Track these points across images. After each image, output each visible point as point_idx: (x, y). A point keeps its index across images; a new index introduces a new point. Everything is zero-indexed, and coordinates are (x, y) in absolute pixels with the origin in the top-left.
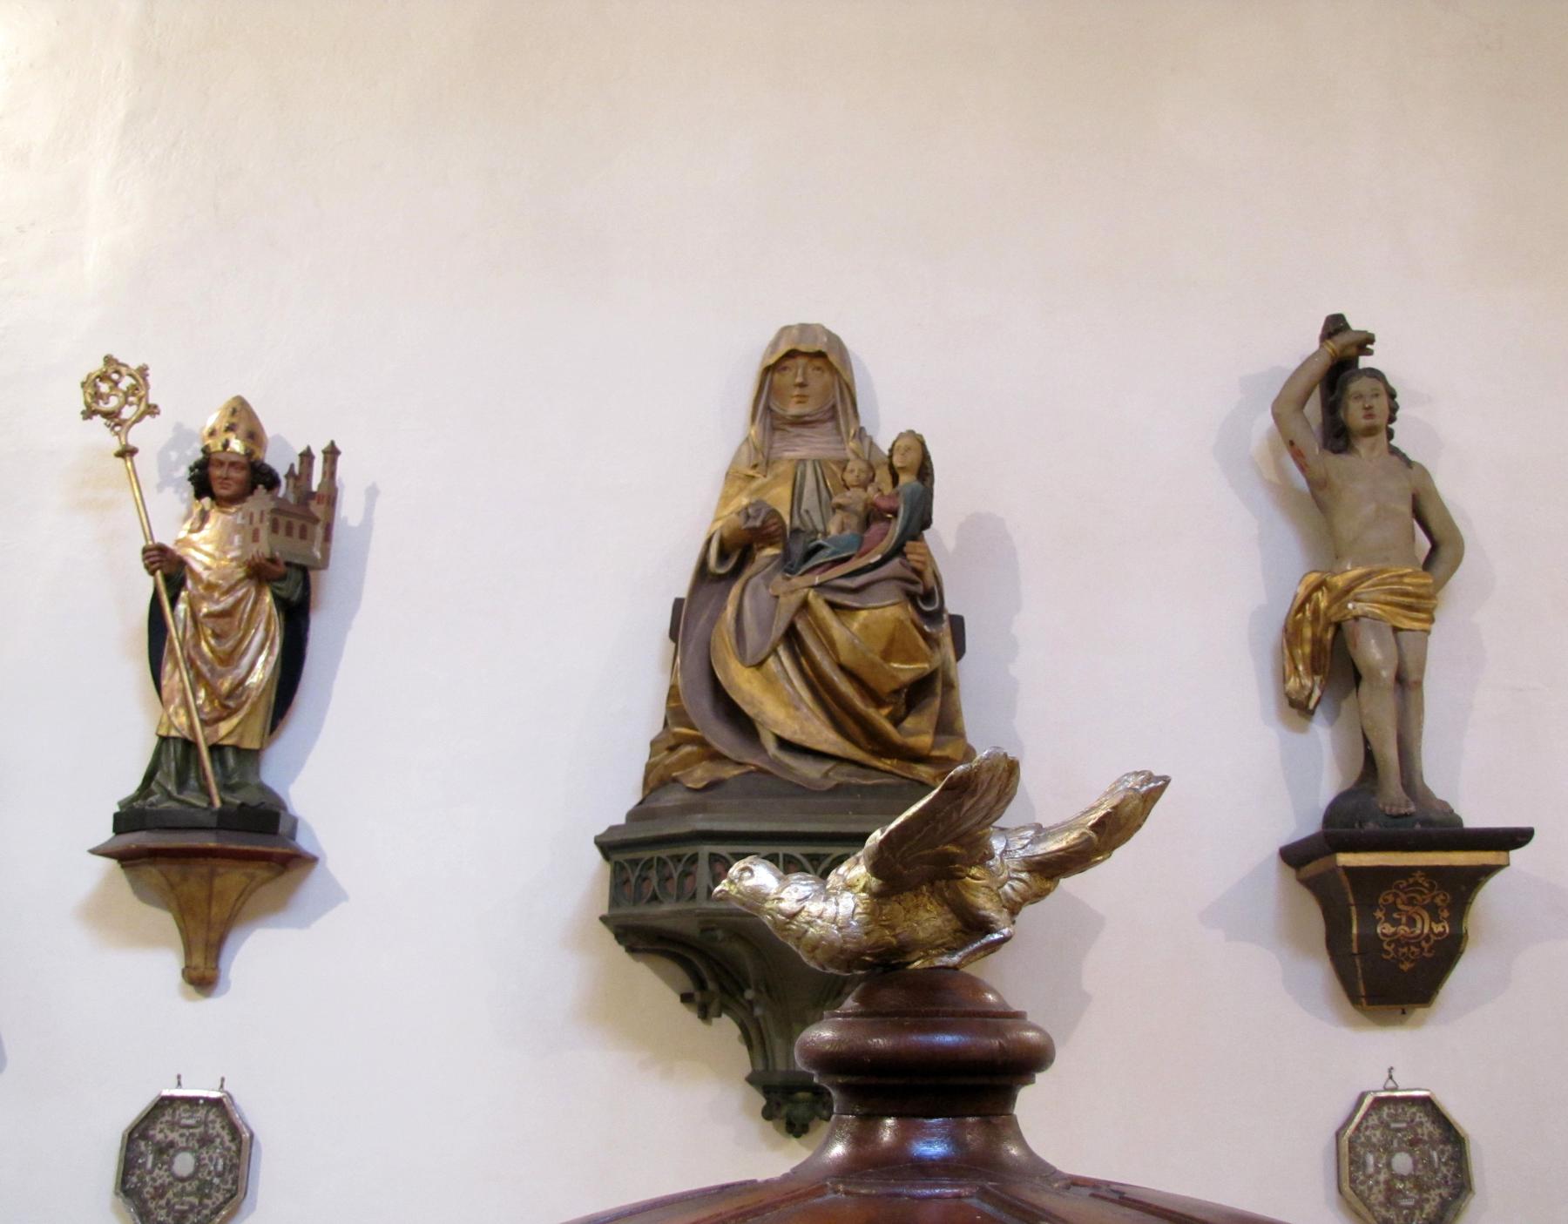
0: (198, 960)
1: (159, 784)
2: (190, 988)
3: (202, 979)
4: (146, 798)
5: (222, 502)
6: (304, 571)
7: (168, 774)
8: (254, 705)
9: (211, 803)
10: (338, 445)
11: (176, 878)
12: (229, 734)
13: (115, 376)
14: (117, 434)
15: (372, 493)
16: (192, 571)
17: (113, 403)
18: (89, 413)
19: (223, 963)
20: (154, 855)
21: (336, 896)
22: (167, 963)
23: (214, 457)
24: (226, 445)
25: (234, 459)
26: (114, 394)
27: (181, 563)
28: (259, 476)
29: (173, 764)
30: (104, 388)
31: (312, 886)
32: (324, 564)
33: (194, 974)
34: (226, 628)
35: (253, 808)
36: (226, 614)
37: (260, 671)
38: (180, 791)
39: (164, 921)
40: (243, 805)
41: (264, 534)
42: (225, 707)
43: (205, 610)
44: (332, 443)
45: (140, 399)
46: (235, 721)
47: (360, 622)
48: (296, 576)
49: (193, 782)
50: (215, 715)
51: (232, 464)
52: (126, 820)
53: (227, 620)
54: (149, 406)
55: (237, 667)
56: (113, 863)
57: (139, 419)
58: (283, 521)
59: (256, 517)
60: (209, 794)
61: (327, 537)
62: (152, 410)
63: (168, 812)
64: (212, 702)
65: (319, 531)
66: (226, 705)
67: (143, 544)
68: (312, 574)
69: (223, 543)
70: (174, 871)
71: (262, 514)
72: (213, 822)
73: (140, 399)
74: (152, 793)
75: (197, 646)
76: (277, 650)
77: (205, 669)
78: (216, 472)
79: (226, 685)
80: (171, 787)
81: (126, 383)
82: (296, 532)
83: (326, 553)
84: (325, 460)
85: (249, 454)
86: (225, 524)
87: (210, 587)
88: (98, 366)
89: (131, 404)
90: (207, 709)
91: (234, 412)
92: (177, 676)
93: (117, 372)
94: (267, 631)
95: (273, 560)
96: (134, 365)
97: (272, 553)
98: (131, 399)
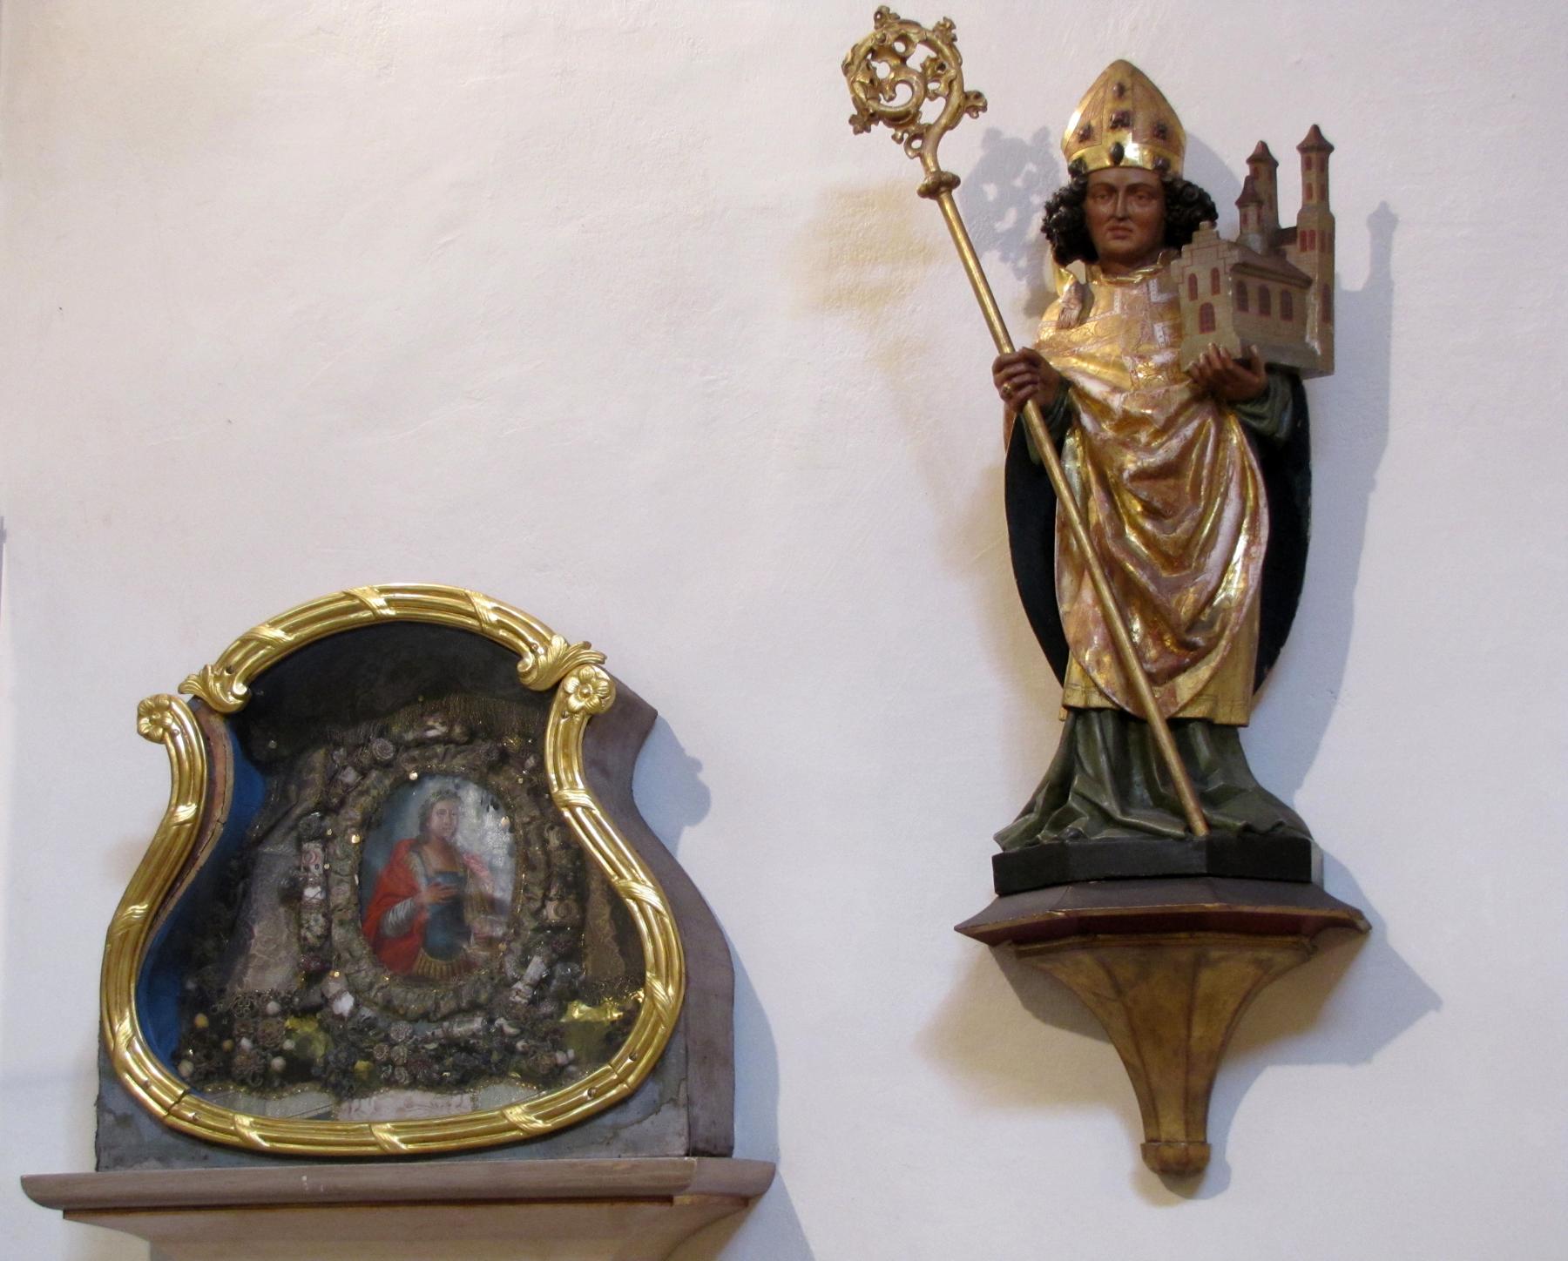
0: (1172, 1127)
1: (1077, 793)
2: (1155, 1179)
3: (1179, 1163)
4: (1058, 825)
5: (1115, 265)
6: (1293, 379)
7: (1098, 779)
8: (1234, 639)
9: (1189, 829)
10: (1329, 134)
11: (1126, 971)
12: (1194, 700)
13: (900, 47)
14: (919, 154)
15: (1383, 223)
16: (1084, 395)
17: (903, 97)
18: (864, 120)
19: (1212, 1137)
20: (1085, 929)
21: (1417, 1000)
22: (1099, 1139)
23: (1095, 180)
24: (1118, 154)
25: (1134, 178)
26: (902, 82)
27: (1065, 384)
28: (1180, 212)
29: (1103, 759)
30: (883, 70)
31: (1364, 981)
32: (1325, 366)
33: (1169, 1153)
34: (1172, 497)
35: (1266, 834)
36: (1169, 471)
37: (1239, 580)
38: (1124, 813)
39: (1102, 1058)
40: (1247, 828)
41: (1224, 313)
42: (1191, 647)
43: (1131, 467)
44: (1316, 130)
45: (950, 84)
46: (1203, 672)
47: (1389, 473)
48: (1283, 389)
49: (1140, 792)
50: (1169, 662)
51: (1132, 189)
52: (1017, 868)
53: (1171, 482)
54: (966, 96)
55: (1200, 570)
56: (981, 948)
57: (953, 122)
58: (1253, 285)
59: (1204, 284)
60: (1180, 813)
61: (1327, 315)
62: (973, 103)
63: (1107, 847)
64: (1158, 639)
65: (1313, 300)
66: (1185, 642)
67: (995, 354)
68: (1312, 386)
69: (1134, 333)
70: (1125, 959)
71: (1215, 274)
72: (1198, 862)
73: (950, 84)
74: (1072, 815)
75: (1120, 534)
76: (1264, 533)
77: (1142, 577)
78: (1101, 208)
79: (1186, 603)
80: (1109, 803)
81: (920, 56)
82: (1276, 306)
83: (1327, 338)
84: (1307, 165)
85: (1162, 168)
86: (1129, 306)
87: (1128, 423)
88: (865, 30)
89: (934, 96)
90: (1152, 653)
91: (1121, 91)
92: (1087, 595)
93: (904, 38)
94: (1243, 498)
95: (1247, 363)
96: (929, 23)
97: (1246, 348)
98: (932, 86)
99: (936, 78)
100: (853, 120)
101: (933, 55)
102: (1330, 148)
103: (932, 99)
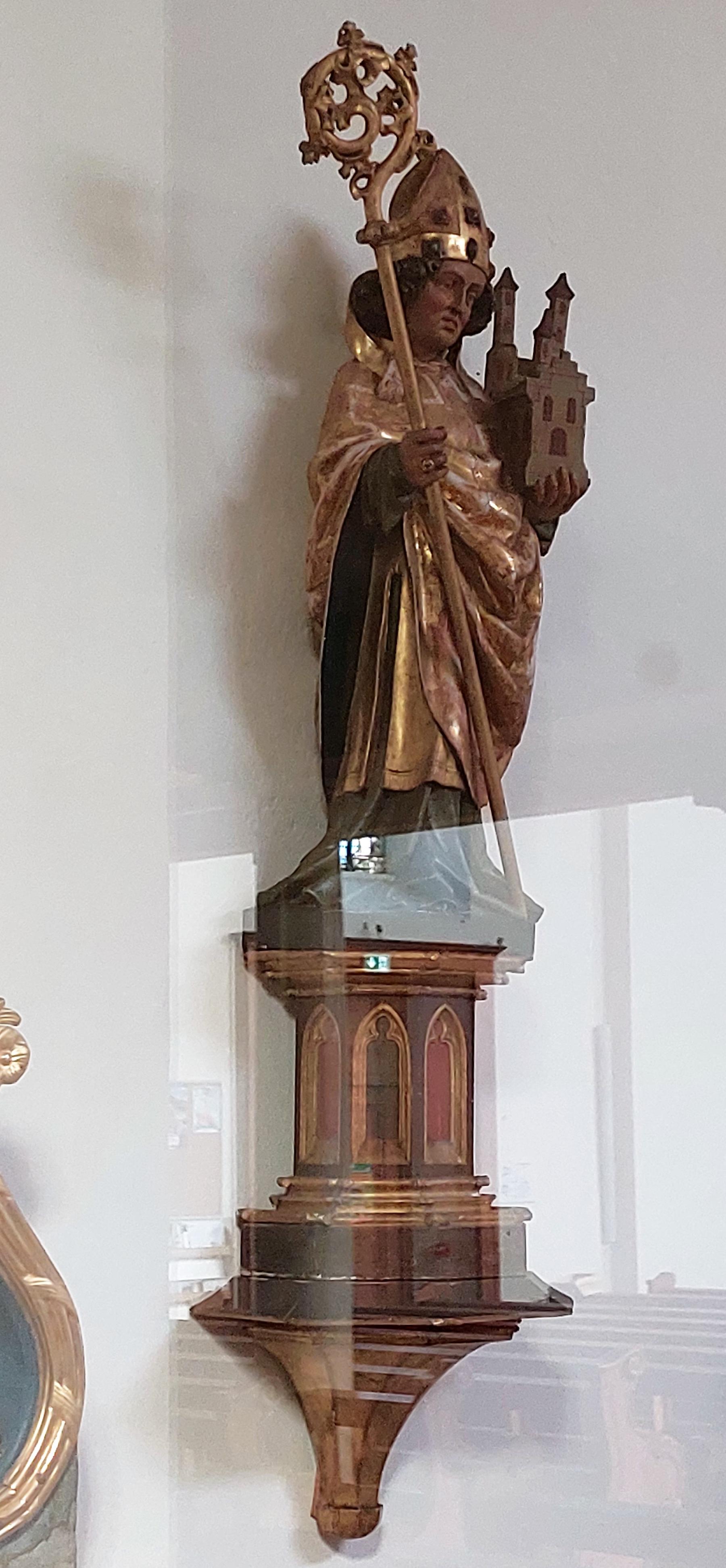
18: (311, 151)
82: (436, 447)
89: (386, 131)
99: (390, 111)
100: (303, 146)
101: (392, 86)
102: (516, 287)
103: (383, 134)
